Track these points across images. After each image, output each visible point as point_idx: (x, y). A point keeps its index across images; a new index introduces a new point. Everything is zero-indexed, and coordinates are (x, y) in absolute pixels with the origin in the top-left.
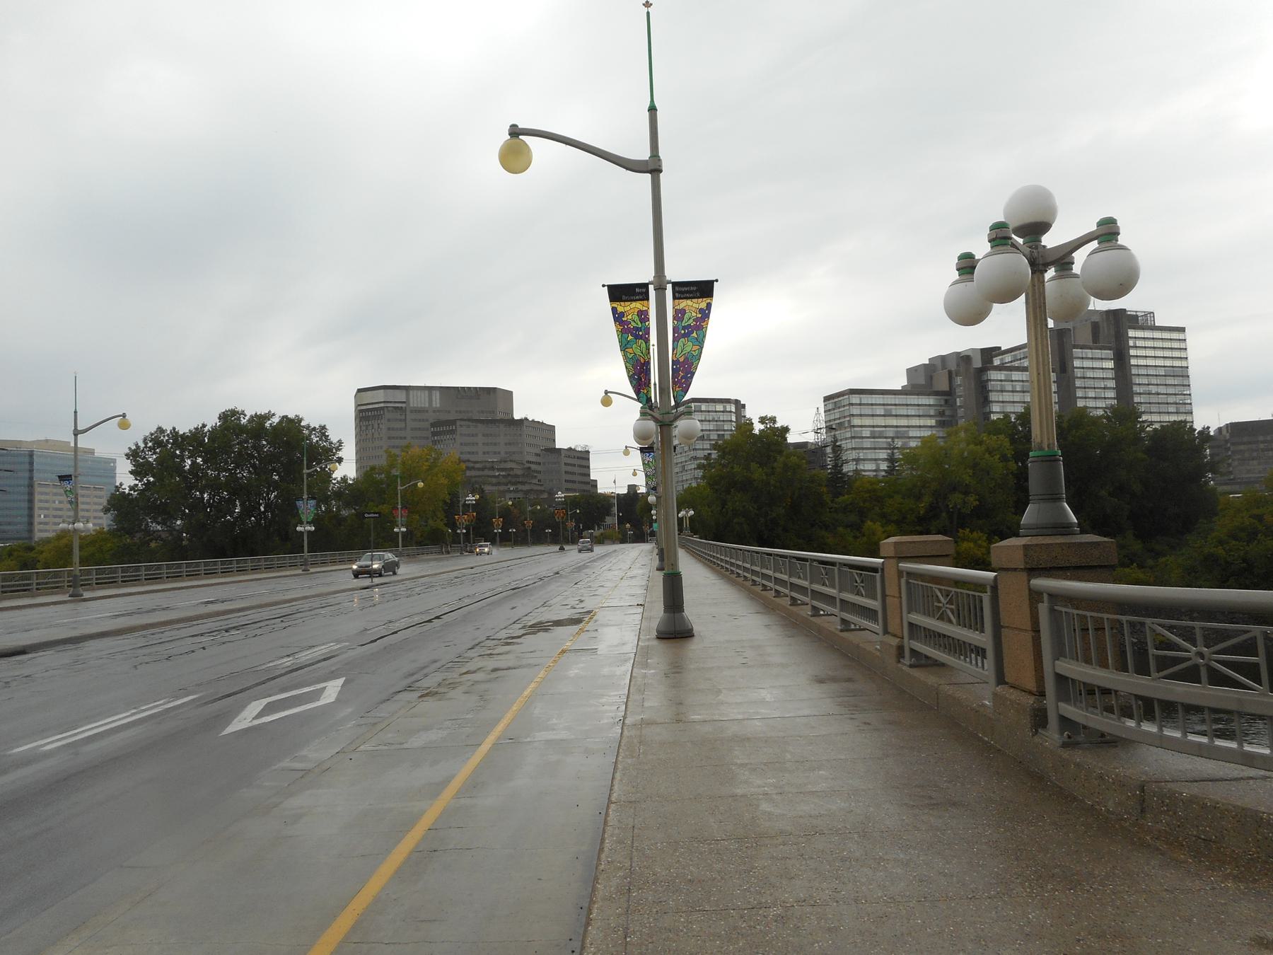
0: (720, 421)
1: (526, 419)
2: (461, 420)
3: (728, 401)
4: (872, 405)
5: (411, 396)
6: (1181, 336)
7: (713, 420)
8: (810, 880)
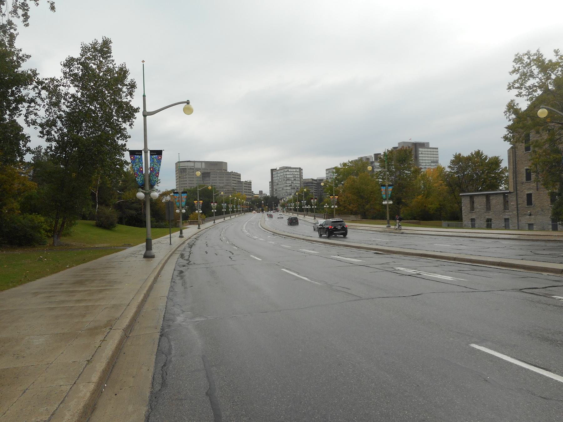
1: (232, 172)
3: (297, 168)
5: (195, 165)
6: (436, 150)
7: (293, 174)
8: (18, 178)
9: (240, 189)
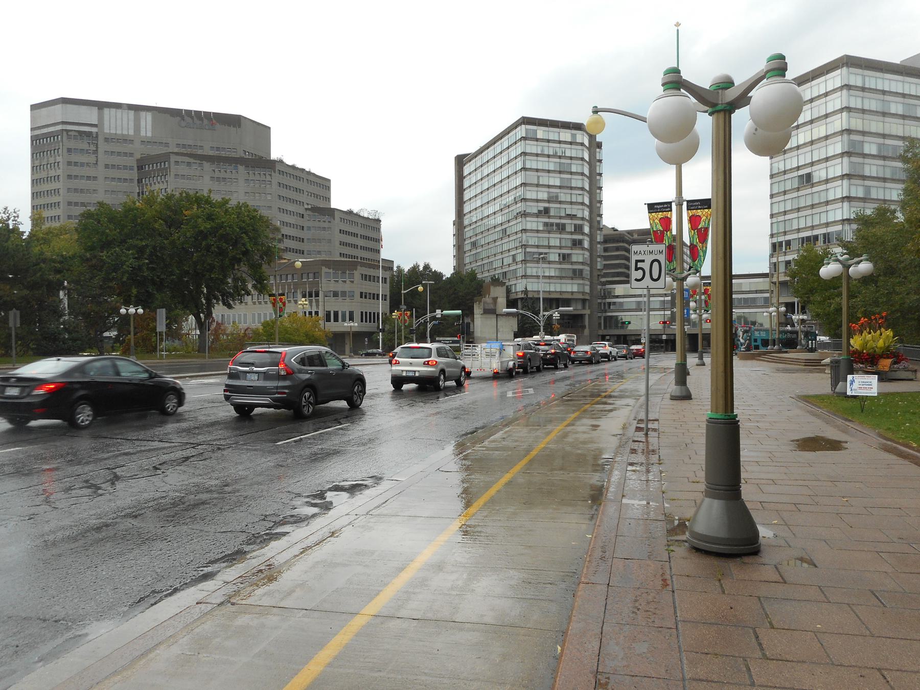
0: (566, 157)
2: (177, 154)
4: (884, 92)
5: (106, 117)
7: (555, 156)
9: (320, 240)
